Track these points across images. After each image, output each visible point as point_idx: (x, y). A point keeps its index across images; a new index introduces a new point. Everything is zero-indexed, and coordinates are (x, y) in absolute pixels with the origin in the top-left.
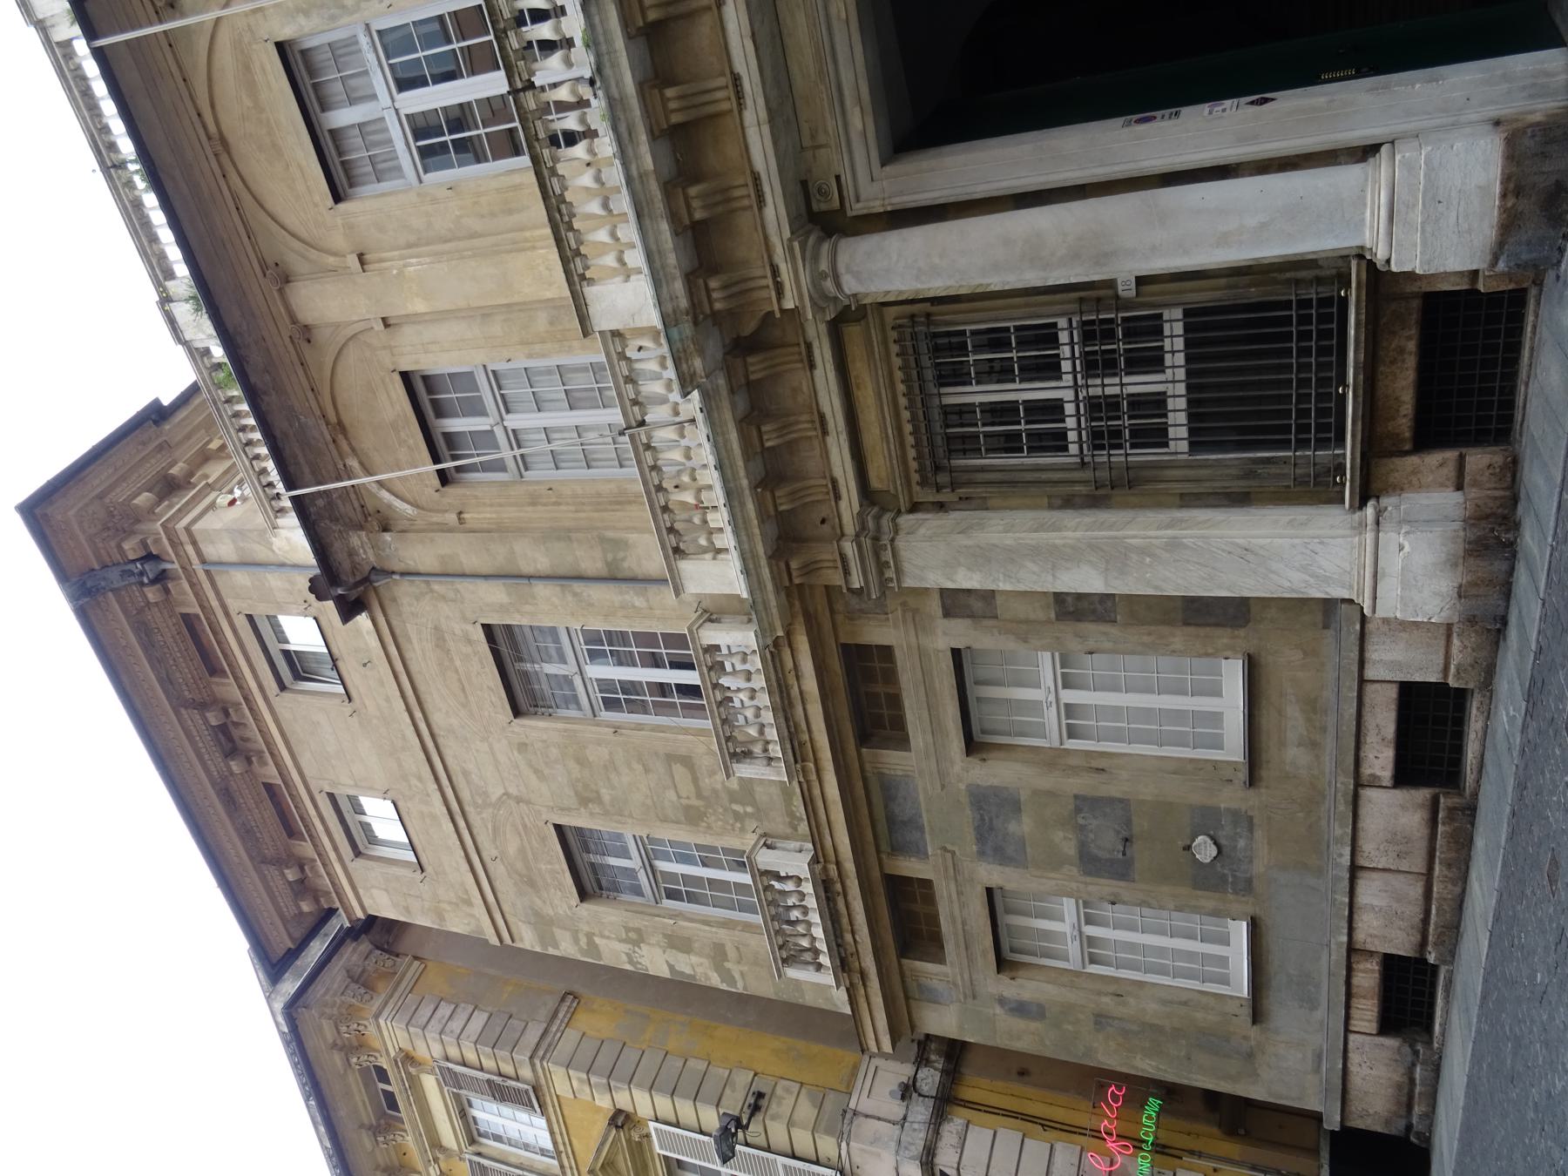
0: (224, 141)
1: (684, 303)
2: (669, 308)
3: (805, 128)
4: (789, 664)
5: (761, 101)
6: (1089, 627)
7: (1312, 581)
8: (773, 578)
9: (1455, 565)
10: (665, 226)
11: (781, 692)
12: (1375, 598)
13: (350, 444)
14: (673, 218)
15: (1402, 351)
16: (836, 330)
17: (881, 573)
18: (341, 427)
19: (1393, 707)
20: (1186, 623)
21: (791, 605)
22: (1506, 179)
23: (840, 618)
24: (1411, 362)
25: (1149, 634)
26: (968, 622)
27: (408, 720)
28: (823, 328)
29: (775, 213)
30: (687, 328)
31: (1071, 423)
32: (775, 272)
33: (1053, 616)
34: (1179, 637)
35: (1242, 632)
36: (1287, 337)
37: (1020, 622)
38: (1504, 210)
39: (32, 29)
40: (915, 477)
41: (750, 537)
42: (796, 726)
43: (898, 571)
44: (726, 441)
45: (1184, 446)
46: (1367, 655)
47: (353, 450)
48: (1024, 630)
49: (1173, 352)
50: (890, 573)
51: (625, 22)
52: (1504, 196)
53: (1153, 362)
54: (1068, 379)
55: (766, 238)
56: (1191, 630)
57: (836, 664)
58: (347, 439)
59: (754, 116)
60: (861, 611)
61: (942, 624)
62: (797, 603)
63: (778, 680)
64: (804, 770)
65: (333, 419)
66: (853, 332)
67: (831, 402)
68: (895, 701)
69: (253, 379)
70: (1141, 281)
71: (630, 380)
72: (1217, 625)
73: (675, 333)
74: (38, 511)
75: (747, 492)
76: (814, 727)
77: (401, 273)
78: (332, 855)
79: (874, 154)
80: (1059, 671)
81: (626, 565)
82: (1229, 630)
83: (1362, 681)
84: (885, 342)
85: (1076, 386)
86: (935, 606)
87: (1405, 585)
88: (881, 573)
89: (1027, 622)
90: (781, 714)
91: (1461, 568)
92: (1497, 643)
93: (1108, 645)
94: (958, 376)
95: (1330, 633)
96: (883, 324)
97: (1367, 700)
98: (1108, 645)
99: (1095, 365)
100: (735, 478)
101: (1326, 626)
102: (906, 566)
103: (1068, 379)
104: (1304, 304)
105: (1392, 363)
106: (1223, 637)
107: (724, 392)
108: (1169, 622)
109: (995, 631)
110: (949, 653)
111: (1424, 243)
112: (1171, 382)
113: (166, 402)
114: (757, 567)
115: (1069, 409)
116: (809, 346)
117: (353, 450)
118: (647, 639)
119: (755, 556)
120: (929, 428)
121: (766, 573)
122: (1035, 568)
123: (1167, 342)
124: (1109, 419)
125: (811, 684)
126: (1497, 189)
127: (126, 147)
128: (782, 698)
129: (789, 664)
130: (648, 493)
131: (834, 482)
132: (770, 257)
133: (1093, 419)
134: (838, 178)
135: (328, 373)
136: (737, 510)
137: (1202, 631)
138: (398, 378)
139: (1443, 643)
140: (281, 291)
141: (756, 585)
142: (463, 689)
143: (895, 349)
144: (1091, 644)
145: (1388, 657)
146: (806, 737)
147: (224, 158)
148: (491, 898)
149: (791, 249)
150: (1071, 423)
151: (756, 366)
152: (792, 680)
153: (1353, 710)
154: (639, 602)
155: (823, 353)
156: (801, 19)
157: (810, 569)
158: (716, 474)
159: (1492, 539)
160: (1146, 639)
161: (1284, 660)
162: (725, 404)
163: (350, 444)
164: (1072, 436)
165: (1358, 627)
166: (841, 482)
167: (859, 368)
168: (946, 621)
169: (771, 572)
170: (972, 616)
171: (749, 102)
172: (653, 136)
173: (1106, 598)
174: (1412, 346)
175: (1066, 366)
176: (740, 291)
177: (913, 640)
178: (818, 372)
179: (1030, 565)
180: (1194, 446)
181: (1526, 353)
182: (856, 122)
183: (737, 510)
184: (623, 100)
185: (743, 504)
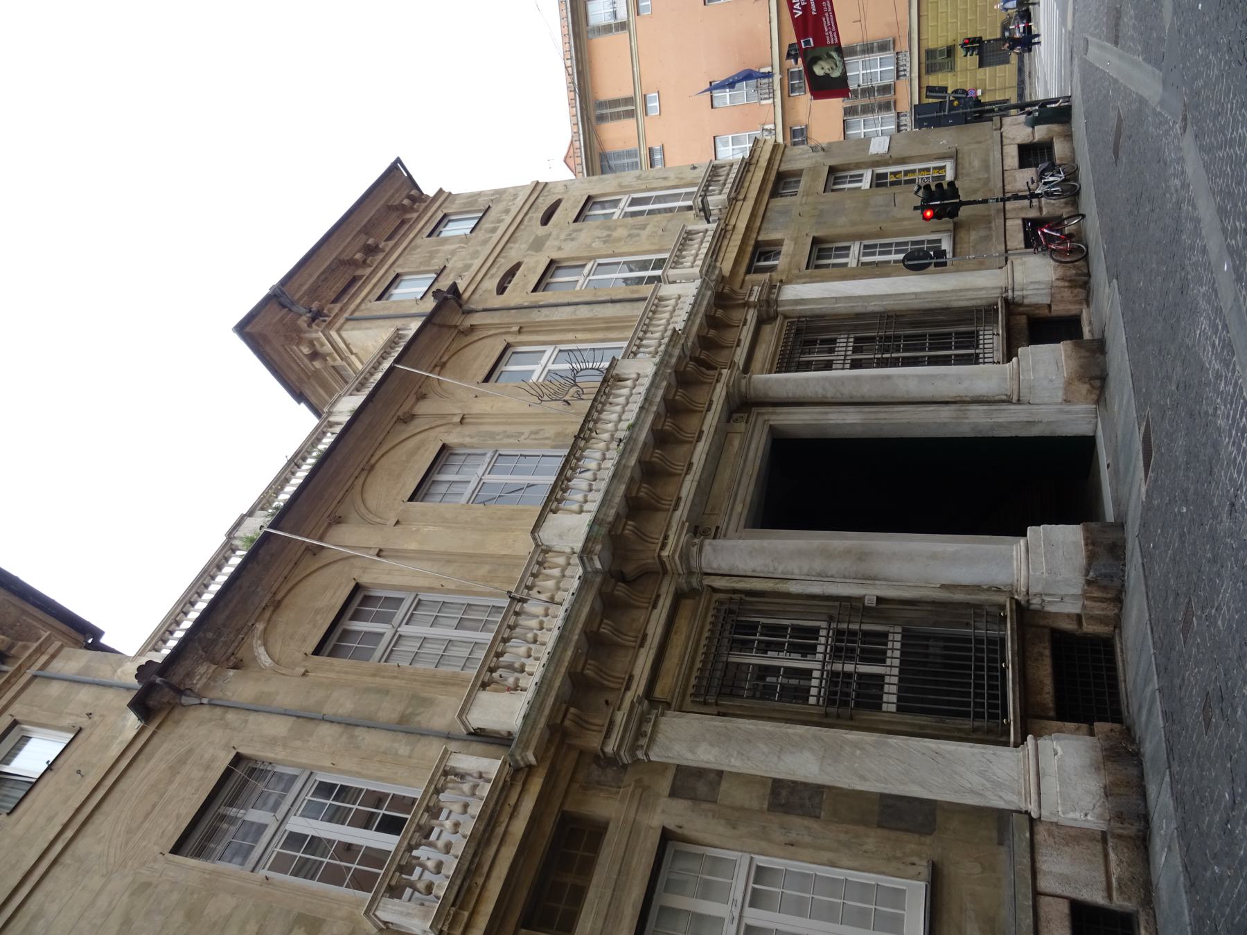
0: (372, 467)
1: (610, 519)
2: (601, 516)
3: (709, 507)
4: (512, 801)
5: (698, 474)
6: (796, 821)
7: (988, 785)
8: (552, 710)
9: (1098, 769)
10: (623, 487)
11: (488, 825)
12: (1039, 794)
13: (270, 617)
14: (628, 489)
15: (1042, 655)
16: (679, 597)
17: (636, 739)
18: (277, 605)
19: (1067, 923)
20: (880, 826)
21: (547, 749)
22: (1086, 539)
23: (575, 786)
24: (1048, 662)
25: (847, 832)
26: (688, 803)
27: (51, 837)
28: (672, 589)
29: (681, 514)
30: (604, 531)
31: (815, 682)
32: (666, 537)
33: (765, 806)
34: (872, 839)
35: (928, 840)
36: (970, 650)
37: (733, 808)
38: (1087, 551)
39: (222, 539)
40: (691, 690)
41: (556, 672)
42: (479, 866)
43: (652, 740)
44: (579, 610)
45: (893, 708)
46: (1038, 865)
47: (269, 620)
48: (735, 817)
49: (893, 649)
50: (643, 742)
51: (653, 424)
52: (1086, 545)
53: (880, 658)
54: (820, 657)
55: (669, 523)
56: (885, 833)
57: (549, 826)
58: (274, 611)
59: (701, 449)
60: (599, 783)
61: (665, 802)
62: (552, 750)
63: (493, 812)
64: (456, 915)
65: (278, 597)
66: (687, 604)
67: (655, 629)
68: (579, 895)
69: (261, 551)
70: (880, 600)
71: (540, 564)
72: (906, 830)
73: (596, 528)
74: (248, 329)
75: (573, 644)
76: (495, 874)
77: (418, 530)
78: (386, 267)
79: (742, 523)
80: (751, 885)
81: (418, 719)
82: (917, 836)
83: (1036, 894)
84: (707, 609)
85: (824, 662)
86: (665, 785)
87: (1062, 783)
88: (636, 739)
89: (742, 809)
90: (473, 845)
91: (1103, 772)
92: (1146, 848)
93: (807, 839)
94: (745, 646)
95: (1003, 849)
96: (710, 601)
97: (1042, 913)
98: (807, 839)
99: (838, 653)
100: (572, 631)
101: (1001, 843)
102: (660, 737)
103: (820, 657)
104: (979, 641)
105: (1037, 660)
106: (911, 843)
107: (596, 586)
108: (864, 822)
109: (710, 814)
110: (660, 831)
111: (1047, 561)
112: (890, 670)
113: (104, 640)
114: (547, 694)
115: (816, 674)
116: (658, 596)
117: (269, 620)
118: (378, 799)
119: (550, 687)
120: (711, 677)
121: (550, 701)
122: (766, 750)
123: (890, 645)
124: (849, 641)
125: (519, 827)
126: (1083, 542)
127: (284, 497)
128: (485, 831)
129: (512, 801)
130: (508, 611)
131: (631, 677)
132: (667, 530)
133: (838, 641)
134: (717, 528)
135: (308, 572)
136: (559, 650)
137: (893, 834)
138: (352, 584)
139: (1101, 861)
140: (330, 525)
141: (537, 705)
142: (147, 816)
143: (710, 619)
144: (793, 836)
145: (1056, 869)
146: (480, 881)
147: (365, 473)
148: (69, 834)
149: (683, 524)
150: (823, 640)
151: (621, 590)
152: (504, 819)
153: (1030, 921)
154: (403, 750)
155: (665, 603)
156: (728, 471)
157: (582, 724)
158: (541, 669)
159: (1123, 756)
160: (843, 837)
161: (966, 873)
162: (590, 598)
163: (270, 617)
164: (814, 691)
165: (1028, 835)
166: (636, 678)
167: (682, 624)
168: (669, 800)
169: (554, 704)
170: (695, 799)
171: (692, 473)
172: (639, 461)
173: (818, 790)
174: (1047, 652)
175: (820, 649)
176: (642, 536)
177: (632, 814)
178: (656, 612)
179: (761, 745)
180: (900, 709)
181: (1120, 664)
182: (739, 508)
183: (559, 650)
184: (635, 441)
185: (565, 649)
